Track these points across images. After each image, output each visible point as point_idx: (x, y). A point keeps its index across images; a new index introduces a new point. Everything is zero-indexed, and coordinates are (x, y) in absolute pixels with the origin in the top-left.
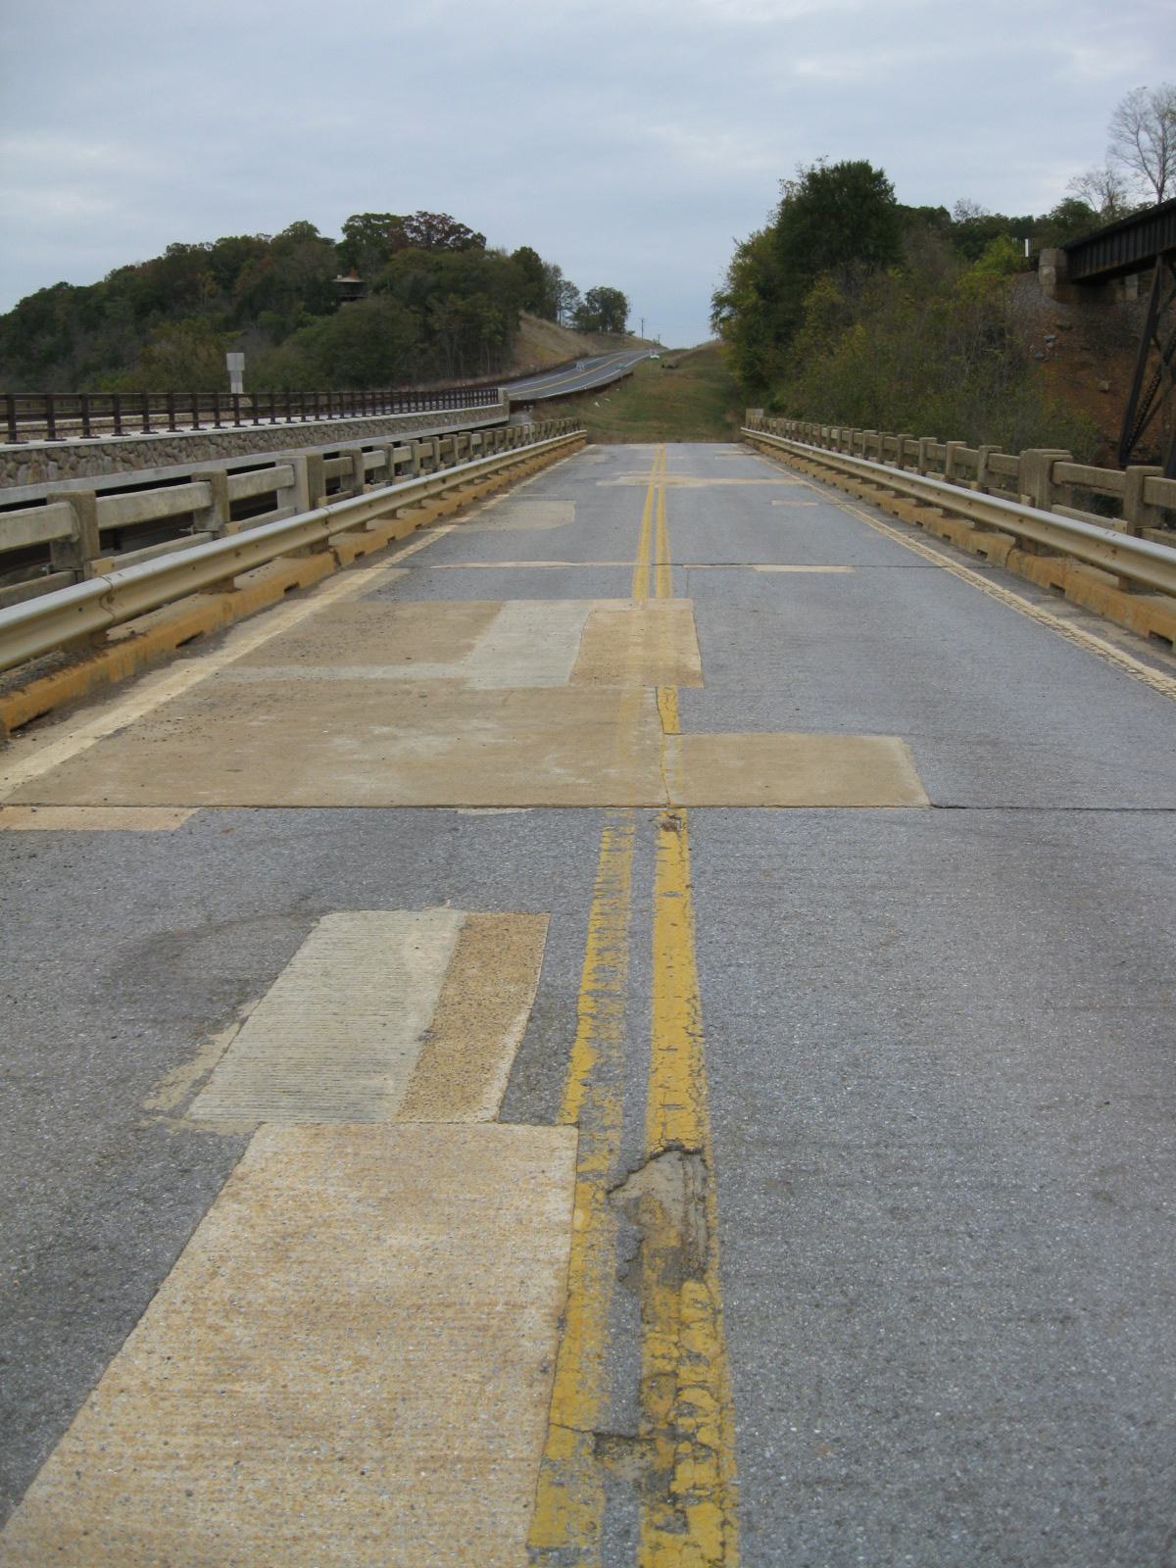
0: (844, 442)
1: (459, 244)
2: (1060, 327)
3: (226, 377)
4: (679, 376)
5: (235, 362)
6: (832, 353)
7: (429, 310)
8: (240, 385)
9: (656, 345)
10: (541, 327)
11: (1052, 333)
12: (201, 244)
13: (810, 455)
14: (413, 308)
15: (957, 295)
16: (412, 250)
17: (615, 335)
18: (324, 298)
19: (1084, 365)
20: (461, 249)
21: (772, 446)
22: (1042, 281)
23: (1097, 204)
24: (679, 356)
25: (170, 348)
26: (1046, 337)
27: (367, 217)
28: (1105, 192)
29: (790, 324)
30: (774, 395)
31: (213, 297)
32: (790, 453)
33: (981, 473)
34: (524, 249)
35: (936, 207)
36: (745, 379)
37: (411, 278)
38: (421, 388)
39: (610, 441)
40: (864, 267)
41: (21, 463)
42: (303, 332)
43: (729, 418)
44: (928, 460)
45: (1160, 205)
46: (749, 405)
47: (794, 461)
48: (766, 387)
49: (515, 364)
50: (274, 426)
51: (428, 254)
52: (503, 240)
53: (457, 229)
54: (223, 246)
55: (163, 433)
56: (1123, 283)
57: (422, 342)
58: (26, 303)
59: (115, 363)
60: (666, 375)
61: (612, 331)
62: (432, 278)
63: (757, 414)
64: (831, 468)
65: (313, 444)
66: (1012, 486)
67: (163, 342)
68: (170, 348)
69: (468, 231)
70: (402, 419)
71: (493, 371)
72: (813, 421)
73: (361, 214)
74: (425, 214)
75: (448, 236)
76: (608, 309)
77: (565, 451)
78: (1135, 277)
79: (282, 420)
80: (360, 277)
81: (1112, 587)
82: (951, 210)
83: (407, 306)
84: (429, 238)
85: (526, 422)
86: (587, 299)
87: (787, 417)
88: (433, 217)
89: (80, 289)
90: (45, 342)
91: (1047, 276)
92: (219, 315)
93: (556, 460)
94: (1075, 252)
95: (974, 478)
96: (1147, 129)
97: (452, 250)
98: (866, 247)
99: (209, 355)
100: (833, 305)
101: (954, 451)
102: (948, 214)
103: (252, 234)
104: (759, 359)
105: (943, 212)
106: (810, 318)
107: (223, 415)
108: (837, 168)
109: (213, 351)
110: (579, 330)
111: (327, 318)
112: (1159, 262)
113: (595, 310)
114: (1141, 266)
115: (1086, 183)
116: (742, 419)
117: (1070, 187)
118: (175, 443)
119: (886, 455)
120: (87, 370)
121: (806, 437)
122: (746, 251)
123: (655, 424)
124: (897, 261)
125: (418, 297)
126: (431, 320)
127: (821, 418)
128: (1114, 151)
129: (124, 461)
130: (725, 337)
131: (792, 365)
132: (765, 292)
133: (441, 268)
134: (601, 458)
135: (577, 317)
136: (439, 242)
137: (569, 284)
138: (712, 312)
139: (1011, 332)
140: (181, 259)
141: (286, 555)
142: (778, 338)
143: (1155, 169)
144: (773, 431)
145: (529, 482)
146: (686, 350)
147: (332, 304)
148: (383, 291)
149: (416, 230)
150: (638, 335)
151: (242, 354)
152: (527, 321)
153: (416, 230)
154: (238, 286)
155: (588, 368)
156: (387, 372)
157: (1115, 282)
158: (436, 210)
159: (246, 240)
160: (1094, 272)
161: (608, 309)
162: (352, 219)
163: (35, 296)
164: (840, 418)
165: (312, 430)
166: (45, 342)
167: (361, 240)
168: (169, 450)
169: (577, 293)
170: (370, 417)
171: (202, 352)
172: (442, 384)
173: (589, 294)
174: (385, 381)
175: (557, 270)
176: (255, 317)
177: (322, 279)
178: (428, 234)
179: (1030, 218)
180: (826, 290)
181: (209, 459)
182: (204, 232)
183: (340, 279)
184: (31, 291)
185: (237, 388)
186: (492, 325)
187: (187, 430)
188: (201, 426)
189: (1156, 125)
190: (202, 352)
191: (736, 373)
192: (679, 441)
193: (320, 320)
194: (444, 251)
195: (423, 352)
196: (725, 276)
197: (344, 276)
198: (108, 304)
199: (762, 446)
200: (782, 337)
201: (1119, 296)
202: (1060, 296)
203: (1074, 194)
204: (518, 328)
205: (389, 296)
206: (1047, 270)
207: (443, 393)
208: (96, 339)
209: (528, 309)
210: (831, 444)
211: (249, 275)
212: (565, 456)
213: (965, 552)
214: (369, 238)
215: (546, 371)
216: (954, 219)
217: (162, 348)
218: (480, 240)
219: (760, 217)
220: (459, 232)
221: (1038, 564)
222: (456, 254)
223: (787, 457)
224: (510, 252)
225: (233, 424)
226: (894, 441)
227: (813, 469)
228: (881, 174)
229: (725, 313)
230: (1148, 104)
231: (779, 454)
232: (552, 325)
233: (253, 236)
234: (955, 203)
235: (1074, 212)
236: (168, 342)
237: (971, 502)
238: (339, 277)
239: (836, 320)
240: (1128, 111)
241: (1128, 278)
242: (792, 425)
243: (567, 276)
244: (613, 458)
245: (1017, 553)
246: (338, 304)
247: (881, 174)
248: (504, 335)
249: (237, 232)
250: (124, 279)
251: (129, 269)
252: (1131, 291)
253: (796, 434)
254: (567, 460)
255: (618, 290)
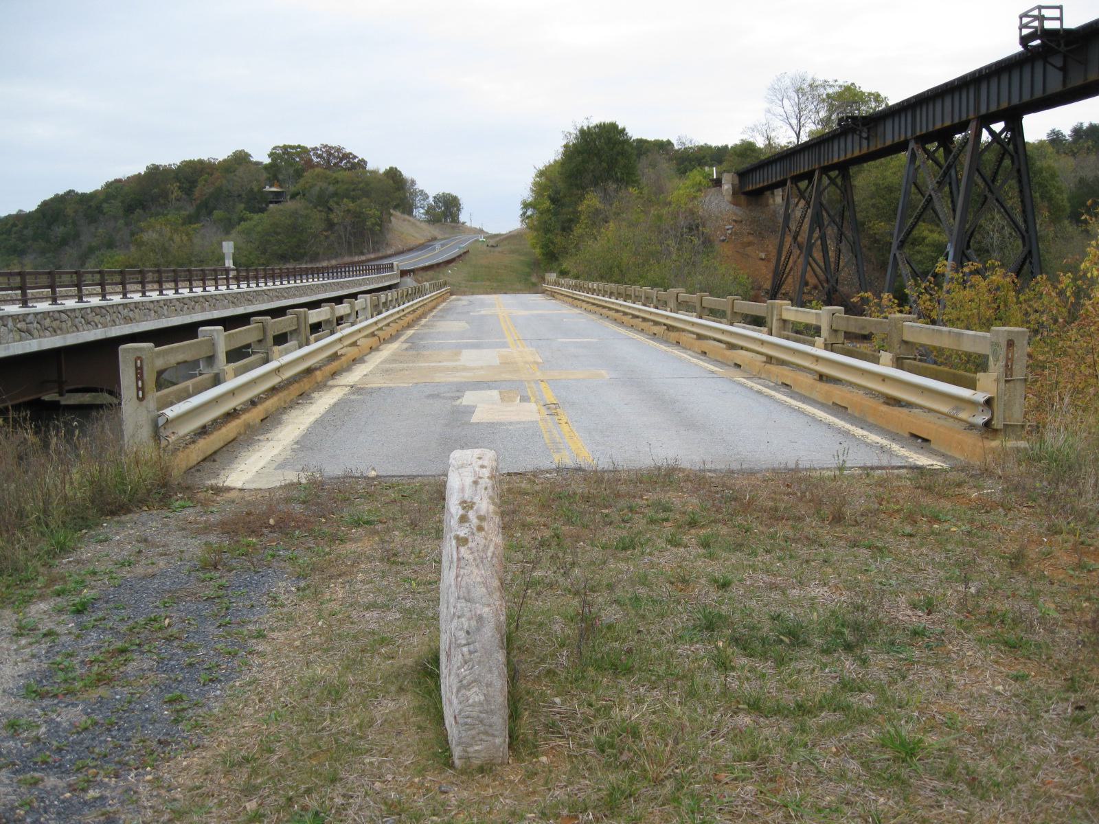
0: (600, 290)
1: (349, 165)
2: (735, 221)
3: (221, 258)
4: (499, 252)
5: (228, 247)
6: (596, 239)
7: (330, 210)
8: (231, 261)
9: (481, 231)
10: (404, 220)
11: (730, 224)
12: (170, 165)
13: (583, 298)
14: (319, 208)
15: (670, 203)
16: (318, 170)
17: (453, 224)
18: (258, 202)
19: (750, 244)
20: (349, 169)
21: (562, 295)
22: (724, 193)
23: (760, 143)
24: (498, 239)
25: (155, 236)
26: (727, 227)
27: (285, 148)
28: (765, 135)
29: (571, 221)
30: (561, 265)
31: (178, 200)
32: (572, 298)
33: (655, 300)
34: (391, 169)
35: (665, 140)
36: (544, 254)
37: (317, 188)
38: (325, 264)
39: (464, 293)
40: (615, 186)
41: (196, 302)
42: (244, 225)
43: (534, 279)
44: (636, 296)
45: (798, 145)
46: (546, 271)
47: (574, 301)
48: (557, 259)
49: (388, 245)
50: (239, 290)
51: (328, 172)
52: (378, 163)
53: (347, 156)
54: (185, 165)
55: (71, 303)
56: (773, 193)
57: (326, 231)
58: (45, 205)
59: (111, 245)
60: (490, 251)
61: (451, 222)
62: (331, 188)
63: (552, 277)
64: (594, 304)
65: (307, 295)
66: (663, 304)
67: (150, 232)
68: (155, 236)
69: (355, 157)
70: (347, 281)
71: (374, 251)
72: (585, 280)
73: (281, 145)
74: (326, 146)
75: (341, 160)
76: (447, 209)
77: (441, 299)
78: (780, 189)
79: (244, 286)
80: (281, 187)
81: (693, 339)
82: (674, 141)
83: (316, 208)
84: (329, 162)
85: (409, 282)
86: (434, 201)
87: (570, 278)
88: (331, 148)
89: (84, 195)
90: (59, 230)
91: (727, 190)
92: (184, 213)
93: (438, 304)
94: (743, 175)
95: (652, 302)
96: (789, 99)
97: (345, 169)
98: (616, 173)
99: (182, 240)
100: (597, 209)
101: (645, 292)
102: (673, 145)
103: (205, 158)
104: (552, 243)
105: (669, 143)
106: (582, 217)
107: (194, 284)
108: (597, 126)
109: (185, 238)
110: (429, 222)
111: (261, 215)
112: (789, 183)
113: (440, 208)
114: (781, 184)
115: (753, 131)
116: (543, 279)
117: (743, 133)
118: (251, 294)
119: (619, 296)
120: (91, 250)
121: (581, 289)
122: (541, 174)
123: (488, 283)
124: (636, 183)
125: (323, 202)
126: (332, 216)
127: (590, 278)
128: (769, 111)
129: (233, 303)
130: (529, 228)
131: (573, 246)
132: (554, 200)
133: (337, 182)
134: (464, 303)
135: (427, 213)
136: (335, 164)
137: (422, 191)
138: (521, 212)
139: (704, 226)
140: (155, 174)
141: (365, 337)
142: (563, 229)
143: (794, 122)
144: (562, 286)
145: (433, 314)
146: (503, 235)
147: (264, 205)
148: (298, 197)
149: (319, 156)
150: (468, 224)
151: (224, 243)
152: (395, 217)
153: (319, 156)
154: (197, 192)
155: (443, 245)
156: (302, 251)
157: (768, 193)
158: (333, 143)
159: (201, 162)
160: (754, 187)
161: (447, 209)
162: (275, 148)
163: (52, 200)
164: (602, 278)
165: (132, 307)
166: (59, 230)
167: (281, 162)
168: (249, 297)
169: (428, 197)
170: (316, 282)
171: (177, 238)
172: (347, 259)
173: (435, 197)
174: (298, 258)
175: (413, 182)
176: (210, 213)
177: (256, 189)
178: (328, 159)
179: (727, 146)
180: (592, 201)
181: (265, 302)
182: (171, 157)
183: (268, 189)
184: (49, 196)
185: (229, 263)
186: (372, 219)
187: (95, 301)
188: (85, 300)
189: (794, 95)
190: (177, 238)
191: (538, 251)
192: (506, 293)
193: (256, 217)
194: (339, 171)
195: (327, 237)
196: (529, 189)
197: (271, 187)
198: (105, 205)
199: (556, 295)
200: (566, 228)
201: (771, 201)
202: (735, 202)
203: (748, 137)
204: (390, 222)
205: (303, 201)
206: (727, 187)
207: (345, 265)
208: (96, 229)
209: (395, 208)
210: (593, 291)
211: (204, 186)
212: (443, 302)
213: (648, 335)
214: (287, 161)
215: (410, 250)
216: (676, 147)
217: (150, 236)
218: (363, 163)
219: (550, 152)
220: (350, 158)
221: (673, 335)
222: (347, 173)
223: (570, 300)
224: (382, 171)
225: (174, 291)
226: (622, 288)
227: (585, 305)
228: (624, 129)
229: (529, 213)
230: (788, 82)
231: (566, 299)
232: (411, 219)
233: (206, 159)
234: (677, 137)
235: (747, 149)
236: (155, 231)
237: (651, 313)
238: (267, 187)
239: (599, 219)
240: (776, 87)
241: (775, 190)
242: (573, 282)
243: (420, 186)
244: (471, 303)
245: (667, 332)
246: (267, 206)
247: (624, 129)
248: (380, 225)
249: (195, 157)
250: (114, 189)
251: (118, 181)
252: (778, 198)
253: (575, 287)
254: (444, 304)
255: (454, 194)
